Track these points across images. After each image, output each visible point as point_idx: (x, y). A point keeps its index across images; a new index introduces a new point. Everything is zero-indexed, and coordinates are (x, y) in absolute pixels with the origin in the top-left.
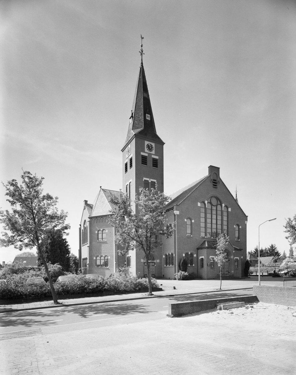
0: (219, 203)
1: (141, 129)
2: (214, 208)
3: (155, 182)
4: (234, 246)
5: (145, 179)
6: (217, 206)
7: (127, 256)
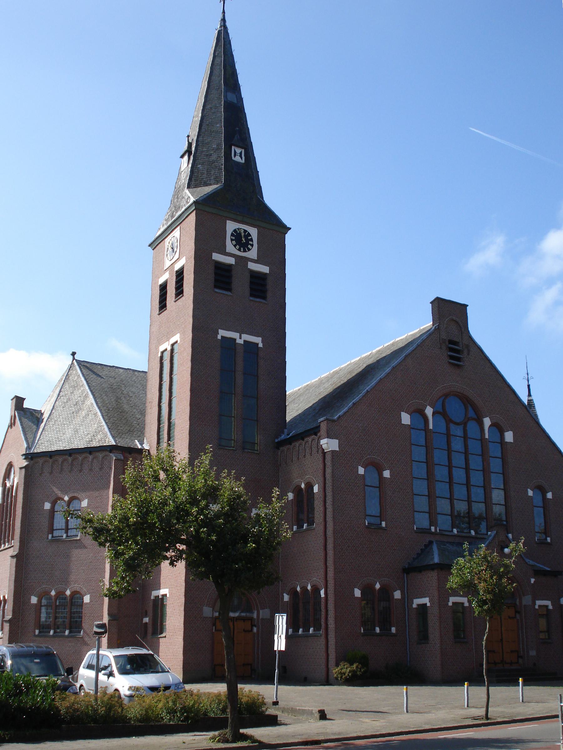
0: (471, 413)
1: (215, 187)
2: (457, 431)
3: (258, 344)
4: (531, 562)
5: (222, 333)
6: (464, 424)
7: (154, 593)
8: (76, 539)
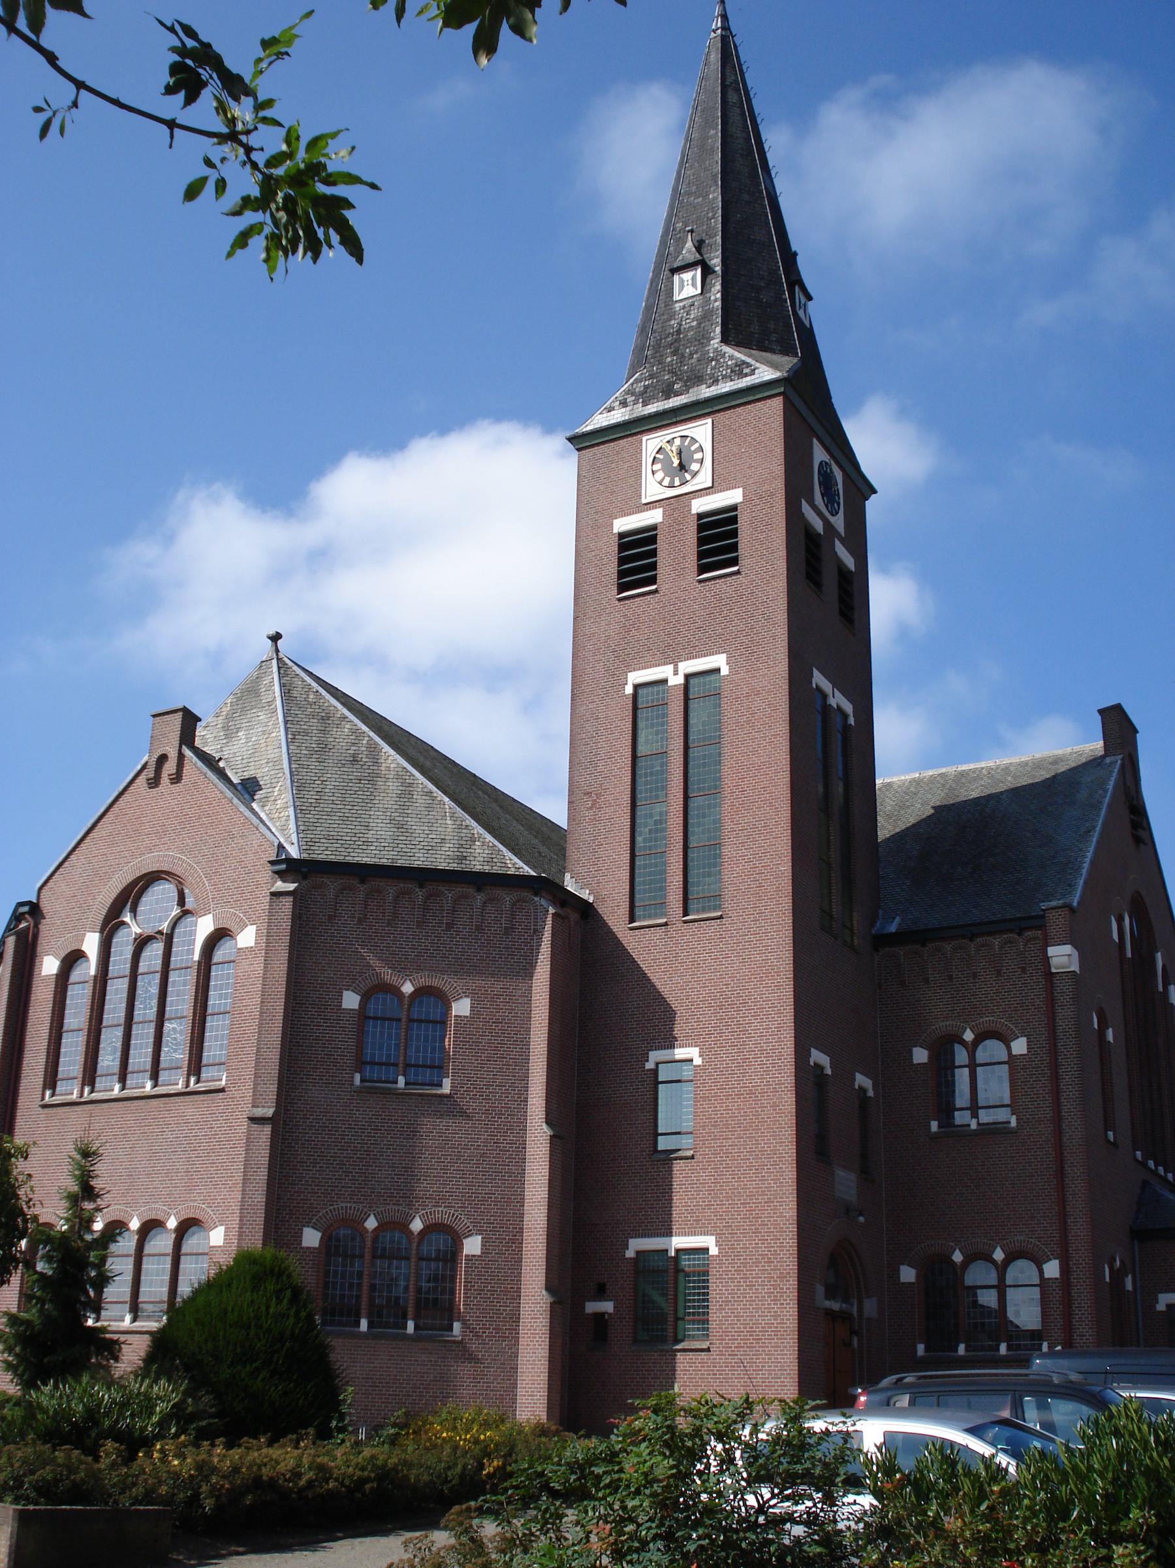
8: (434, 1092)
